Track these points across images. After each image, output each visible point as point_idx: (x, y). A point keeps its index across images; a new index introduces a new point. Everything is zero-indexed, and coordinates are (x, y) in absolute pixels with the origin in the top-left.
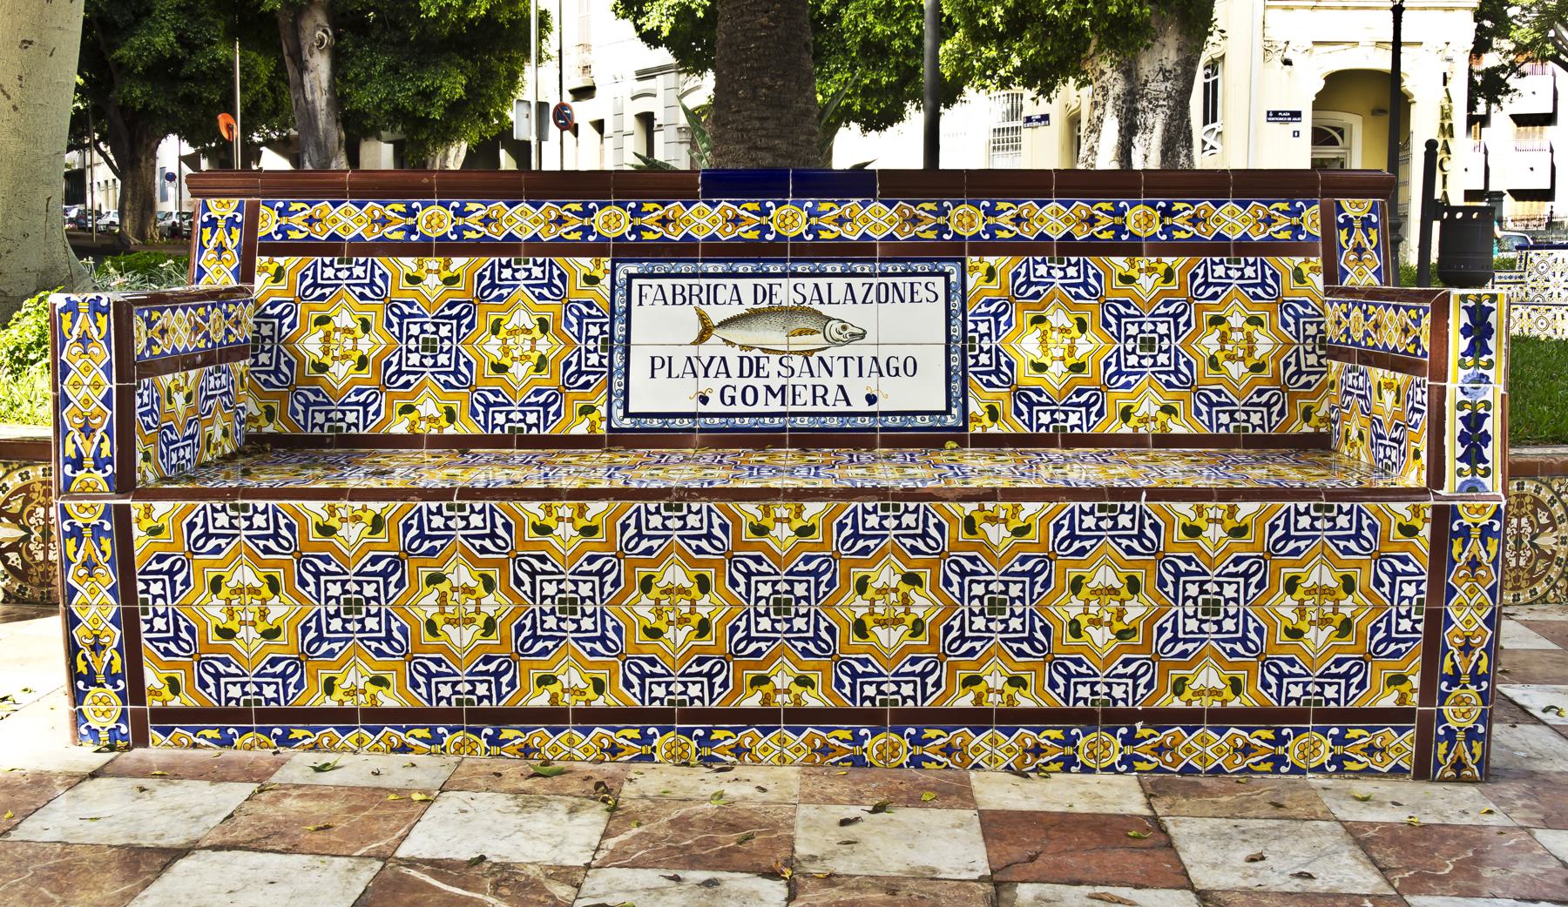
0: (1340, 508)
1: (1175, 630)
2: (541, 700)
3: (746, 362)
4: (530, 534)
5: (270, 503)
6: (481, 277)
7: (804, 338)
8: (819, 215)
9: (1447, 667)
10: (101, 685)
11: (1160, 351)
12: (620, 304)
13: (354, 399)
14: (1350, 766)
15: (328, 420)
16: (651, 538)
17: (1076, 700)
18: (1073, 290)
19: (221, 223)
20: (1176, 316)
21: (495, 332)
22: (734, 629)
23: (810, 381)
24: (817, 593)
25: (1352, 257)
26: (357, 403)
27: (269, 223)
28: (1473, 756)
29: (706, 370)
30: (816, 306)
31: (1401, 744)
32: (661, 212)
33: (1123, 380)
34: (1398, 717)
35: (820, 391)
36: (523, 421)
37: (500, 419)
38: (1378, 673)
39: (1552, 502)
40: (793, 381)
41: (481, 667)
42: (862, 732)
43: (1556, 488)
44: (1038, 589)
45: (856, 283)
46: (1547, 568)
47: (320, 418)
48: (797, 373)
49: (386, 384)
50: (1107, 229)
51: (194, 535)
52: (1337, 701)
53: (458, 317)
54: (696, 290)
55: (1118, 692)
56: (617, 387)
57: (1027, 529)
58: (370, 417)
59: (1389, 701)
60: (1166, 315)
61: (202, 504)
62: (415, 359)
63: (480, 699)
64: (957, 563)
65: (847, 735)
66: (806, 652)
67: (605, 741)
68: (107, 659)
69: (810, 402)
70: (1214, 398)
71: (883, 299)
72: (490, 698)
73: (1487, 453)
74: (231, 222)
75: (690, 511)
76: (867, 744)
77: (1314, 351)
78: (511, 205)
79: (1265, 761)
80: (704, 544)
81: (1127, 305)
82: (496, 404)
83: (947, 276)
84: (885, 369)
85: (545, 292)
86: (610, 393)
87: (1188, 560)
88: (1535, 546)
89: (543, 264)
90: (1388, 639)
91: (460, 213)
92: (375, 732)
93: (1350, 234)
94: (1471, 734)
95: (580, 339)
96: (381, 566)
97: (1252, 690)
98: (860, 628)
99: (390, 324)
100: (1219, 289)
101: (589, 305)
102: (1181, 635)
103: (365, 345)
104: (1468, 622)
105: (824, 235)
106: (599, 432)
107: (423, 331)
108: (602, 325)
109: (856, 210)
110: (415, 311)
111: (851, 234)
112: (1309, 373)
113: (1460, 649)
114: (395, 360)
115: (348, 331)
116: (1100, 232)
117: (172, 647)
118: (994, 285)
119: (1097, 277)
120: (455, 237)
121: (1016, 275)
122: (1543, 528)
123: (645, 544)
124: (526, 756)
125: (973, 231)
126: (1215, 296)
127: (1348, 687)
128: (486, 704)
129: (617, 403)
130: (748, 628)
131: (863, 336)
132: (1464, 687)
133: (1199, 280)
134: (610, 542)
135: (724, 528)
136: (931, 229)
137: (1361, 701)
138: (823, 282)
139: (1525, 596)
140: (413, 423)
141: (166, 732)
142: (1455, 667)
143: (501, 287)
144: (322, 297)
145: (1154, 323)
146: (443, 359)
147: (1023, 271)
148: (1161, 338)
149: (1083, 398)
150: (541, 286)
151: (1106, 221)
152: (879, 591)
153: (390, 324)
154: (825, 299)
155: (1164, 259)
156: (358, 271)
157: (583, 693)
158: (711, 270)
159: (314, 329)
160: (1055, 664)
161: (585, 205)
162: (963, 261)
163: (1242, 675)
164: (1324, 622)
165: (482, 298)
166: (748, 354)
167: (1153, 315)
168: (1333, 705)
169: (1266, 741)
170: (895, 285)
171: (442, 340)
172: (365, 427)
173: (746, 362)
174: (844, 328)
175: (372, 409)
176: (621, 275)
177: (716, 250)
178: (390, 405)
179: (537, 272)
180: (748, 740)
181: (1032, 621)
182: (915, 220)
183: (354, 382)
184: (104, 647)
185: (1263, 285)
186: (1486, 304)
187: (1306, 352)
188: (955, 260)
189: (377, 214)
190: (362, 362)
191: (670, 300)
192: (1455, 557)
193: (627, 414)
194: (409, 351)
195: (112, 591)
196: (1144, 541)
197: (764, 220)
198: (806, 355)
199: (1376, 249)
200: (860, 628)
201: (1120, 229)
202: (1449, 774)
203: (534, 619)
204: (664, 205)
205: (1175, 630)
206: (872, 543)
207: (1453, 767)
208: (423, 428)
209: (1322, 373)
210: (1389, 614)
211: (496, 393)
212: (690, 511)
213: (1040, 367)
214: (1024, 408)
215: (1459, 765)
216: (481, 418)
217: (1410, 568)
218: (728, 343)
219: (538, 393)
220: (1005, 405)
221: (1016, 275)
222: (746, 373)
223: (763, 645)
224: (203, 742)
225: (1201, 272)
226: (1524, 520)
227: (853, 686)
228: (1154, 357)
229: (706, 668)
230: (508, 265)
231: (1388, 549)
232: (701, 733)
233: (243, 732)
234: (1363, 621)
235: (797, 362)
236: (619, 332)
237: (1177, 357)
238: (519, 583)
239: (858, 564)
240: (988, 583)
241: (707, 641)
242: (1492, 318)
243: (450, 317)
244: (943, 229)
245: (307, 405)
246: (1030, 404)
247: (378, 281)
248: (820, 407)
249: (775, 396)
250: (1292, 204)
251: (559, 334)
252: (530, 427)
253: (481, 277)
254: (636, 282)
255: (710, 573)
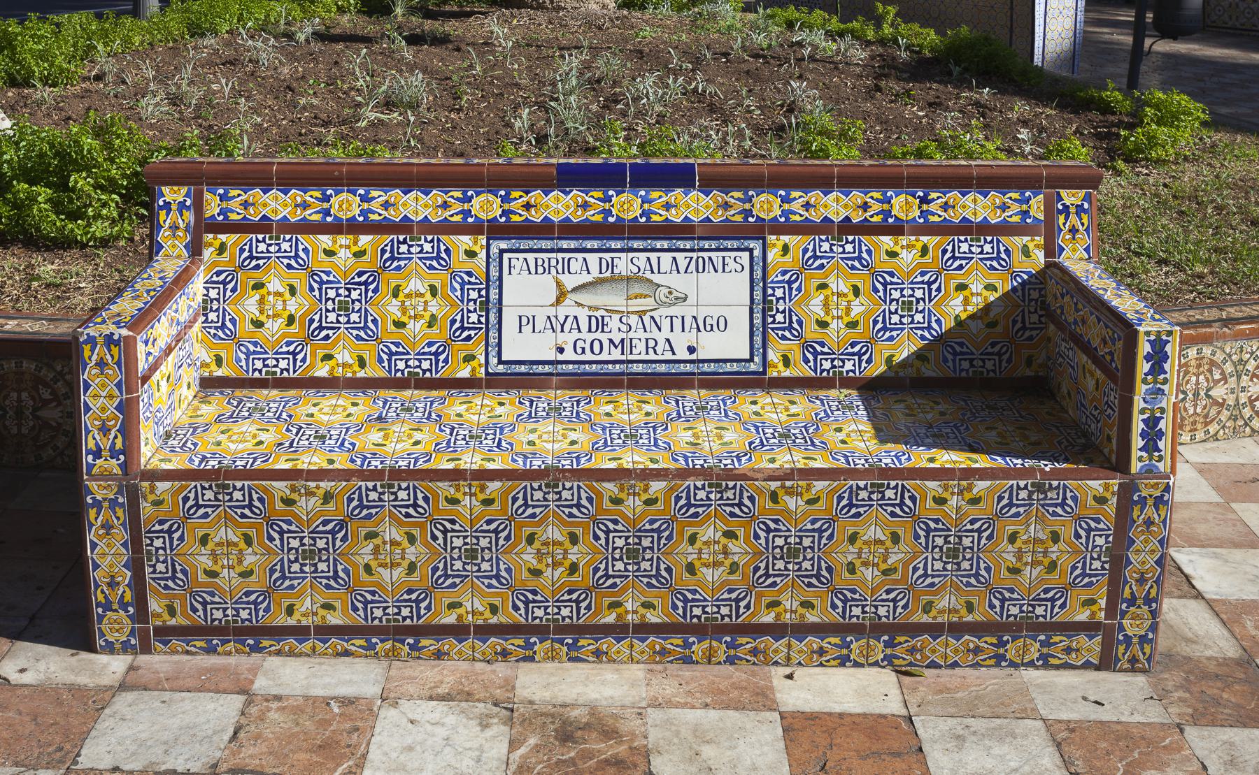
0: (1050, 485)
1: (925, 568)
2: (450, 619)
3: (593, 320)
4: (443, 504)
5: (246, 483)
6: (383, 251)
7: (639, 301)
8: (650, 202)
9: (1127, 593)
10: (116, 611)
11: (917, 311)
12: (494, 274)
13: (285, 349)
14: (1052, 661)
15: (265, 366)
16: (534, 507)
17: (851, 617)
18: (850, 263)
19: (174, 207)
20: (929, 283)
21: (395, 295)
22: (596, 570)
23: (643, 335)
24: (659, 544)
25: (1068, 237)
26: (288, 353)
27: (213, 206)
28: (1144, 654)
29: (562, 326)
30: (648, 275)
31: (1091, 646)
32: (525, 199)
33: (888, 334)
34: (1090, 628)
35: (651, 344)
36: (419, 367)
37: (401, 365)
38: (1076, 596)
39: (55, 448)
40: (631, 335)
41: (406, 597)
42: (691, 640)
43: (1228, 351)
44: (824, 541)
45: (680, 256)
46: (1219, 413)
47: (259, 365)
48: (633, 329)
49: (311, 337)
50: (877, 214)
51: (187, 506)
52: (1045, 617)
53: (366, 283)
54: (553, 262)
55: (882, 611)
56: (493, 340)
57: (816, 500)
58: (299, 363)
59: (1083, 616)
60: (922, 282)
61: (193, 484)
62: (332, 317)
63: (404, 619)
64: (764, 523)
65: (679, 642)
66: (649, 585)
67: (499, 648)
68: (120, 592)
69: (644, 352)
70: (958, 349)
71: (701, 269)
72: (412, 618)
73: (1161, 444)
74: (182, 205)
75: (564, 488)
76: (694, 648)
77: (1036, 312)
78: (405, 193)
79: (990, 658)
80: (574, 511)
81: (892, 274)
82: (397, 353)
83: (751, 251)
84: (701, 326)
85: (435, 263)
86: (487, 345)
87: (937, 521)
88: (1208, 396)
89: (432, 241)
90: (1084, 575)
91: (365, 199)
92: (325, 642)
93: (1066, 219)
94: (1143, 639)
95: (462, 301)
96: (329, 527)
97: (981, 610)
98: (691, 568)
99: (312, 289)
100: (964, 262)
101: (469, 274)
102: (930, 572)
103: (293, 306)
104: (1143, 563)
105: (655, 218)
106: (478, 376)
107: (338, 295)
108: (480, 290)
109: (680, 197)
110: (331, 278)
111: (676, 217)
112: (1032, 329)
113: (1137, 581)
114: (317, 318)
115: (278, 294)
116: (872, 216)
117: (170, 583)
118: (788, 258)
119: (869, 252)
120: (361, 219)
121: (805, 251)
122: (1217, 382)
123: (530, 511)
124: (439, 659)
125: (772, 215)
126: (961, 267)
127: (1053, 607)
128: (408, 621)
129: (493, 352)
130: (606, 569)
131: (685, 299)
132: (1139, 607)
133: (948, 255)
134: (503, 510)
135: (590, 500)
136: (739, 213)
137: (1061, 617)
138: (653, 256)
139: (1200, 435)
140: (332, 369)
141: (165, 643)
142: (1132, 593)
143: (399, 259)
144: (257, 267)
145: (912, 289)
146: (354, 317)
147: (811, 247)
148: (918, 301)
149: (856, 349)
150: (431, 259)
151: (876, 207)
152: (705, 543)
153: (312, 289)
154: (656, 270)
155: (922, 238)
156: (285, 246)
157: (482, 614)
158: (565, 246)
159: (253, 293)
160: (836, 592)
161: (464, 193)
162: (764, 239)
163: (974, 599)
164: (1034, 563)
165: (384, 268)
166: (595, 313)
167: (912, 283)
168: (1041, 619)
169: (992, 644)
170: (710, 258)
171: (353, 302)
172: (295, 372)
173: (593, 320)
174: (670, 293)
175: (300, 357)
176: (494, 250)
177: (569, 230)
178: (314, 354)
179: (427, 247)
180: (605, 646)
181: (819, 563)
182: (726, 206)
183: (284, 335)
184: (118, 584)
185: (998, 258)
186: (1164, 337)
187: (1030, 312)
188: (757, 239)
189: (299, 199)
190: (291, 320)
191: (533, 270)
192: (1135, 517)
193: (500, 362)
194: (327, 311)
195: (125, 545)
196: (904, 507)
197: (607, 206)
198: (641, 314)
199: (1087, 230)
200: (691, 568)
201: (887, 214)
202: (1127, 666)
203: (446, 563)
204: (527, 193)
205: (925, 568)
206: (700, 510)
207: (1129, 661)
208: (339, 372)
209: (1041, 329)
210: (1085, 558)
211: (397, 344)
212: (564, 488)
213: (823, 324)
214: (810, 357)
215: (1134, 660)
216: (386, 364)
217: (1101, 526)
218: (579, 305)
219: (430, 344)
220: (796, 354)
221: (805, 251)
222: (594, 329)
223: (618, 581)
224: (193, 649)
225: (950, 248)
226: (1201, 377)
227: (685, 609)
228: (912, 316)
229: (574, 596)
230: (405, 242)
231: (1084, 513)
232: (570, 641)
233: (224, 642)
234: (1065, 562)
235: (634, 320)
236: (494, 296)
237: (929, 316)
238: (434, 538)
239: (690, 525)
240: (786, 537)
241: (576, 578)
242: (1168, 348)
243: (359, 284)
244: (748, 213)
245: (248, 354)
246: (815, 354)
247: (302, 254)
248: (652, 356)
249: (616, 347)
250: (1022, 194)
251: (446, 297)
252: (424, 371)
253: (383, 251)
254: (506, 256)
255: (579, 531)
